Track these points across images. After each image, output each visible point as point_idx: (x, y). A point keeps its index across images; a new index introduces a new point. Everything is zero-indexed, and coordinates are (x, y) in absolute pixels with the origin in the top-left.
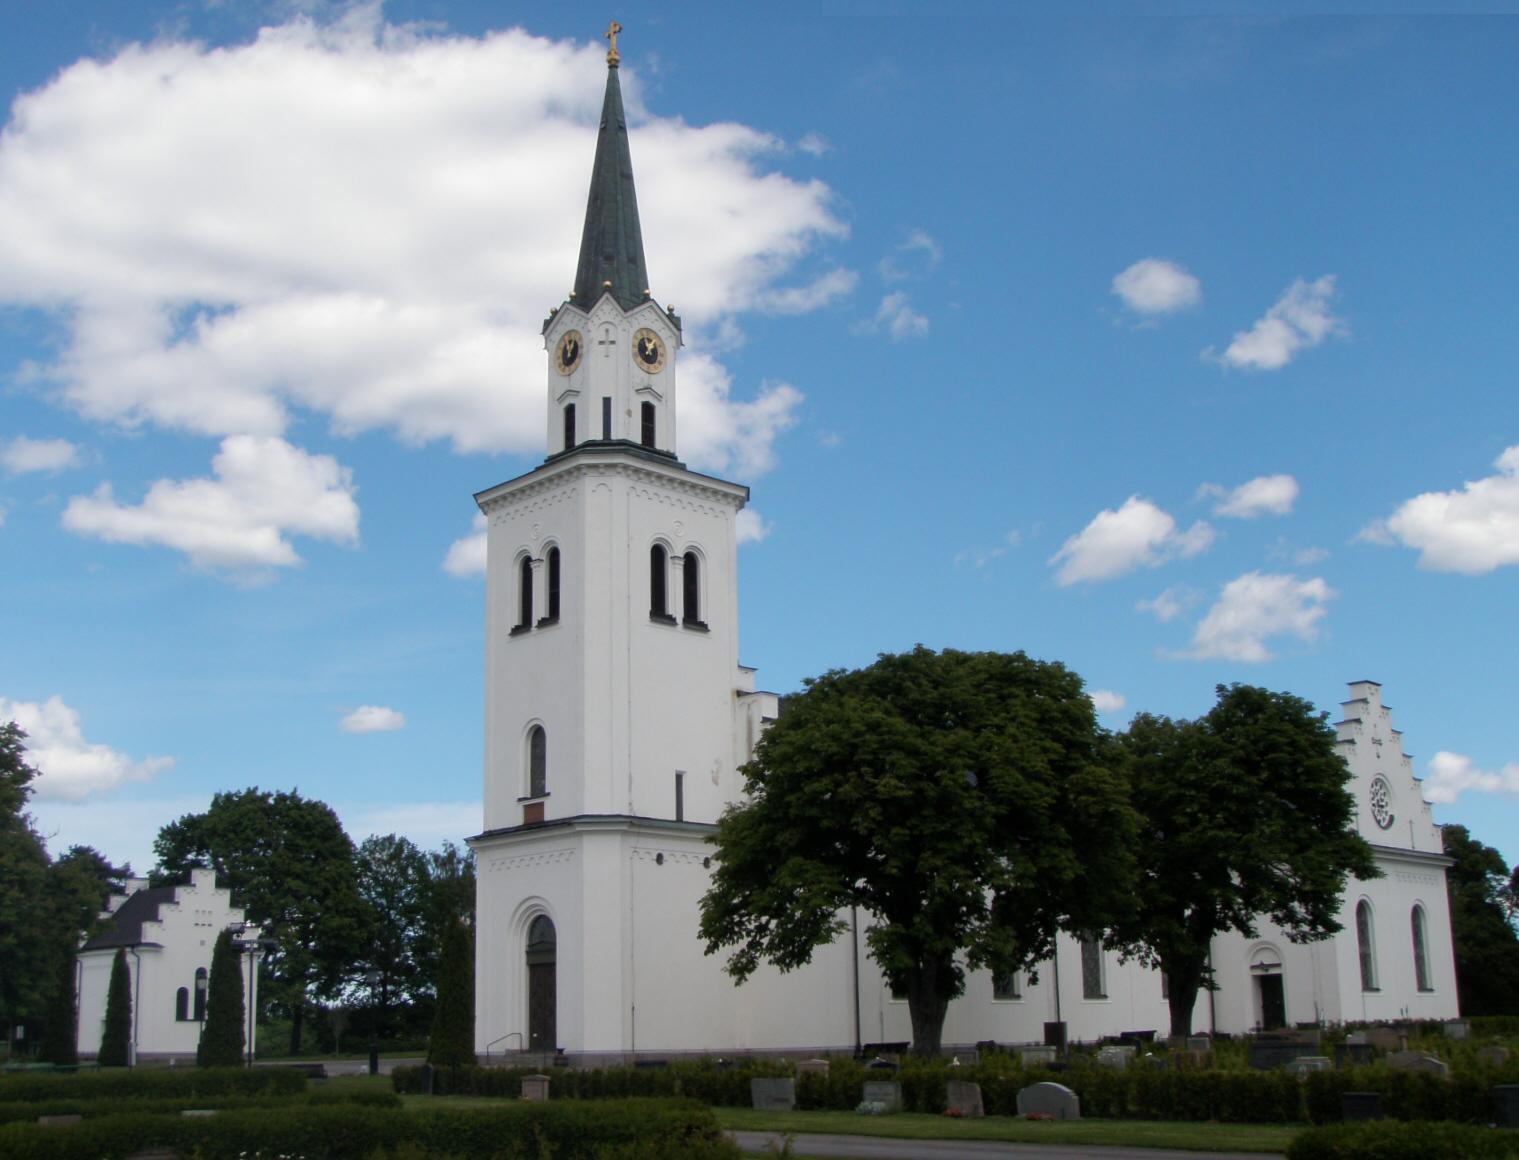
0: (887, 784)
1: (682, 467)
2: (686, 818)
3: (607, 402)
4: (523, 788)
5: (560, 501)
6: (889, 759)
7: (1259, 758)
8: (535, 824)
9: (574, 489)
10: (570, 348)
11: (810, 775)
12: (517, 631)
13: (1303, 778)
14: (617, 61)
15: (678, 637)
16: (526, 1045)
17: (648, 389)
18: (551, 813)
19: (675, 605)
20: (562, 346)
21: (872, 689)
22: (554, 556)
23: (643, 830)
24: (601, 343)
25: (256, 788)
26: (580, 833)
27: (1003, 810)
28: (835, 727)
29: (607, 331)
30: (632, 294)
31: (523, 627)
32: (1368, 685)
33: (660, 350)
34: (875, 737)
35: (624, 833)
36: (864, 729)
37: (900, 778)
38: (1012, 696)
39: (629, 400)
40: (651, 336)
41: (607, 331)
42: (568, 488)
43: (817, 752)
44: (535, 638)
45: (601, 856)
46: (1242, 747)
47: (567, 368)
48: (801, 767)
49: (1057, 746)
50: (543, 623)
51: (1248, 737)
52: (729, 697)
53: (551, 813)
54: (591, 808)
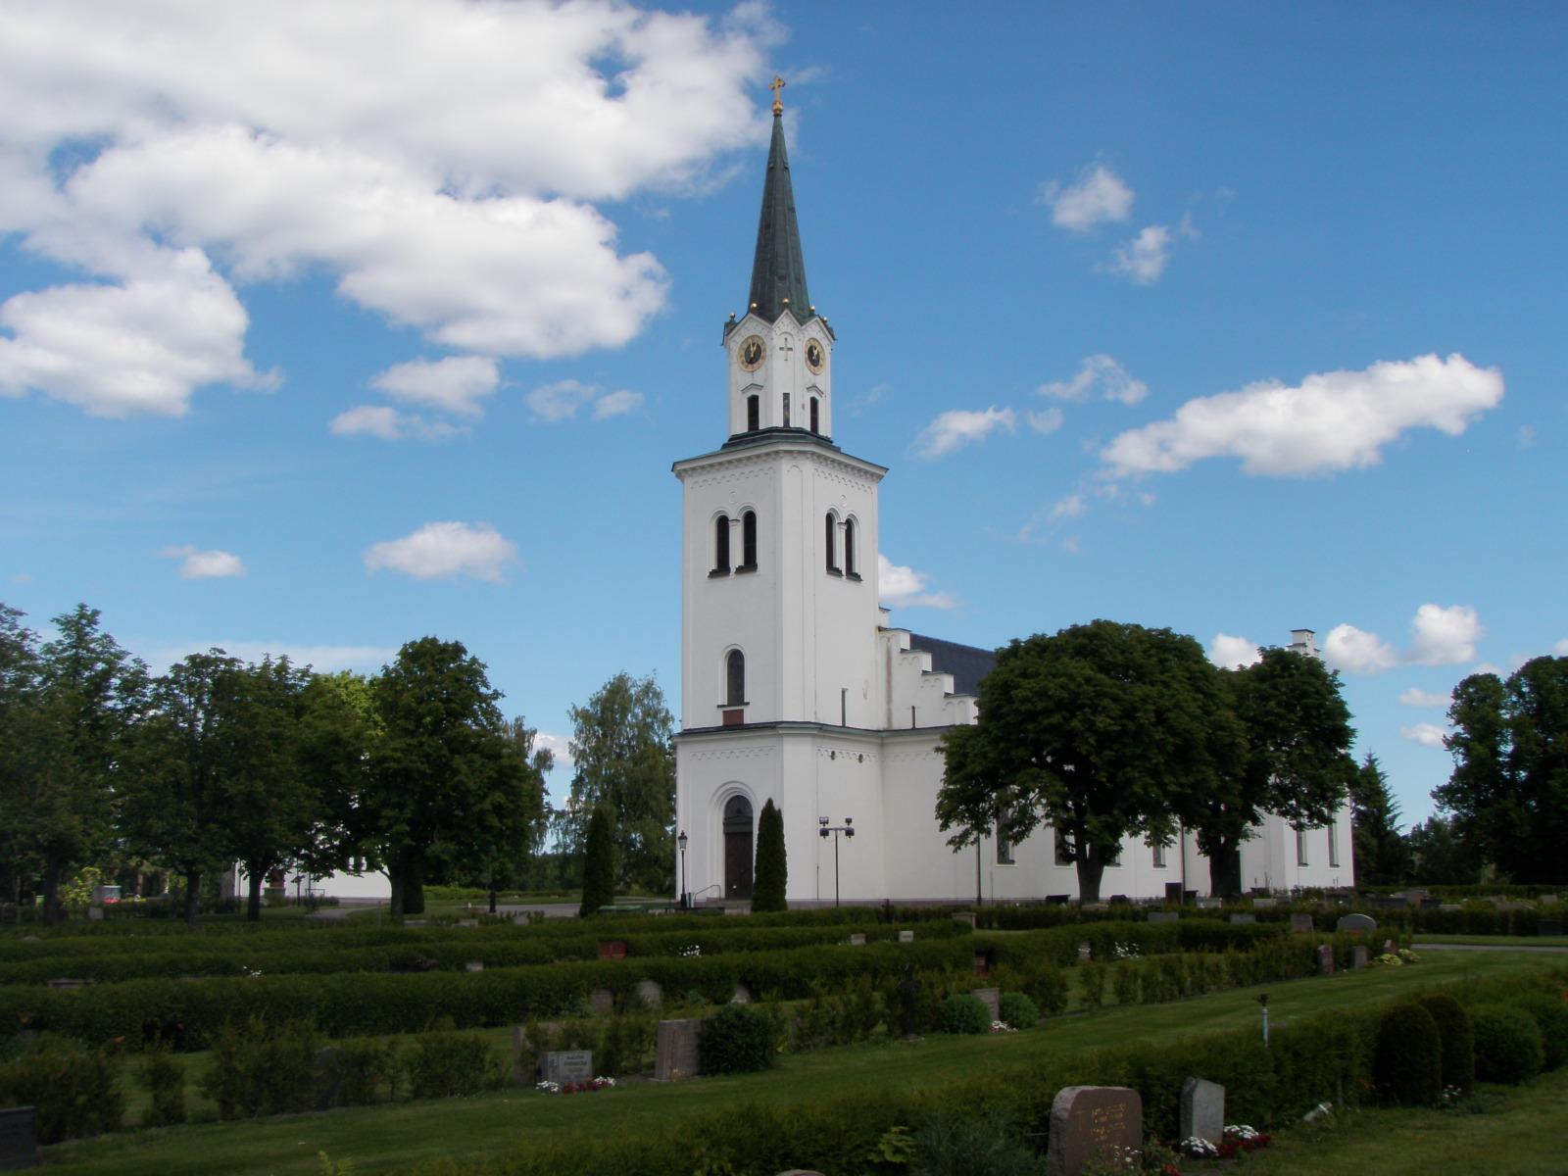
0: (1102, 722)
1: (837, 450)
2: (847, 725)
3: (786, 396)
4: (722, 697)
5: (756, 476)
6: (1102, 704)
7: (1296, 702)
8: (734, 725)
9: (771, 468)
10: (753, 349)
11: (1048, 712)
12: (713, 574)
13: (1324, 717)
14: (781, 110)
15: (843, 584)
16: (723, 895)
17: (814, 387)
18: (750, 717)
19: (840, 562)
20: (745, 346)
21: (1192, 678)
22: (750, 520)
23: (826, 734)
24: (781, 349)
25: (332, 674)
26: (781, 735)
27: (1178, 741)
28: (1063, 680)
29: (786, 339)
30: (799, 309)
31: (722, 568)
32: (1307, 633)
33: (821, 355)
34: (1091, 689)
35: (813, 736)
36: (1083, 682)
37: (1112, 718)
38: (1166, 660)
39: (803, 396)
40: (816, 345)
41: (786, 339)
42: (765, 466)
43: (1050, 697)
44: (732, 581)
45: (797, 754)
46: (1285, 694)
47: (750, 366)
48: (1040, 706)
49: (1201, 696)
50: (740, 570)
51: (1287, 687)
52: (874, 630)
53: (750, 717)
54: (789, 716)
